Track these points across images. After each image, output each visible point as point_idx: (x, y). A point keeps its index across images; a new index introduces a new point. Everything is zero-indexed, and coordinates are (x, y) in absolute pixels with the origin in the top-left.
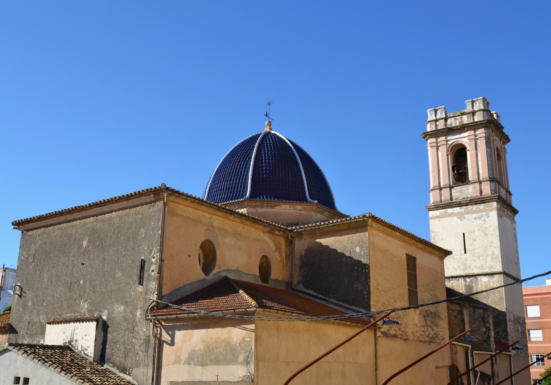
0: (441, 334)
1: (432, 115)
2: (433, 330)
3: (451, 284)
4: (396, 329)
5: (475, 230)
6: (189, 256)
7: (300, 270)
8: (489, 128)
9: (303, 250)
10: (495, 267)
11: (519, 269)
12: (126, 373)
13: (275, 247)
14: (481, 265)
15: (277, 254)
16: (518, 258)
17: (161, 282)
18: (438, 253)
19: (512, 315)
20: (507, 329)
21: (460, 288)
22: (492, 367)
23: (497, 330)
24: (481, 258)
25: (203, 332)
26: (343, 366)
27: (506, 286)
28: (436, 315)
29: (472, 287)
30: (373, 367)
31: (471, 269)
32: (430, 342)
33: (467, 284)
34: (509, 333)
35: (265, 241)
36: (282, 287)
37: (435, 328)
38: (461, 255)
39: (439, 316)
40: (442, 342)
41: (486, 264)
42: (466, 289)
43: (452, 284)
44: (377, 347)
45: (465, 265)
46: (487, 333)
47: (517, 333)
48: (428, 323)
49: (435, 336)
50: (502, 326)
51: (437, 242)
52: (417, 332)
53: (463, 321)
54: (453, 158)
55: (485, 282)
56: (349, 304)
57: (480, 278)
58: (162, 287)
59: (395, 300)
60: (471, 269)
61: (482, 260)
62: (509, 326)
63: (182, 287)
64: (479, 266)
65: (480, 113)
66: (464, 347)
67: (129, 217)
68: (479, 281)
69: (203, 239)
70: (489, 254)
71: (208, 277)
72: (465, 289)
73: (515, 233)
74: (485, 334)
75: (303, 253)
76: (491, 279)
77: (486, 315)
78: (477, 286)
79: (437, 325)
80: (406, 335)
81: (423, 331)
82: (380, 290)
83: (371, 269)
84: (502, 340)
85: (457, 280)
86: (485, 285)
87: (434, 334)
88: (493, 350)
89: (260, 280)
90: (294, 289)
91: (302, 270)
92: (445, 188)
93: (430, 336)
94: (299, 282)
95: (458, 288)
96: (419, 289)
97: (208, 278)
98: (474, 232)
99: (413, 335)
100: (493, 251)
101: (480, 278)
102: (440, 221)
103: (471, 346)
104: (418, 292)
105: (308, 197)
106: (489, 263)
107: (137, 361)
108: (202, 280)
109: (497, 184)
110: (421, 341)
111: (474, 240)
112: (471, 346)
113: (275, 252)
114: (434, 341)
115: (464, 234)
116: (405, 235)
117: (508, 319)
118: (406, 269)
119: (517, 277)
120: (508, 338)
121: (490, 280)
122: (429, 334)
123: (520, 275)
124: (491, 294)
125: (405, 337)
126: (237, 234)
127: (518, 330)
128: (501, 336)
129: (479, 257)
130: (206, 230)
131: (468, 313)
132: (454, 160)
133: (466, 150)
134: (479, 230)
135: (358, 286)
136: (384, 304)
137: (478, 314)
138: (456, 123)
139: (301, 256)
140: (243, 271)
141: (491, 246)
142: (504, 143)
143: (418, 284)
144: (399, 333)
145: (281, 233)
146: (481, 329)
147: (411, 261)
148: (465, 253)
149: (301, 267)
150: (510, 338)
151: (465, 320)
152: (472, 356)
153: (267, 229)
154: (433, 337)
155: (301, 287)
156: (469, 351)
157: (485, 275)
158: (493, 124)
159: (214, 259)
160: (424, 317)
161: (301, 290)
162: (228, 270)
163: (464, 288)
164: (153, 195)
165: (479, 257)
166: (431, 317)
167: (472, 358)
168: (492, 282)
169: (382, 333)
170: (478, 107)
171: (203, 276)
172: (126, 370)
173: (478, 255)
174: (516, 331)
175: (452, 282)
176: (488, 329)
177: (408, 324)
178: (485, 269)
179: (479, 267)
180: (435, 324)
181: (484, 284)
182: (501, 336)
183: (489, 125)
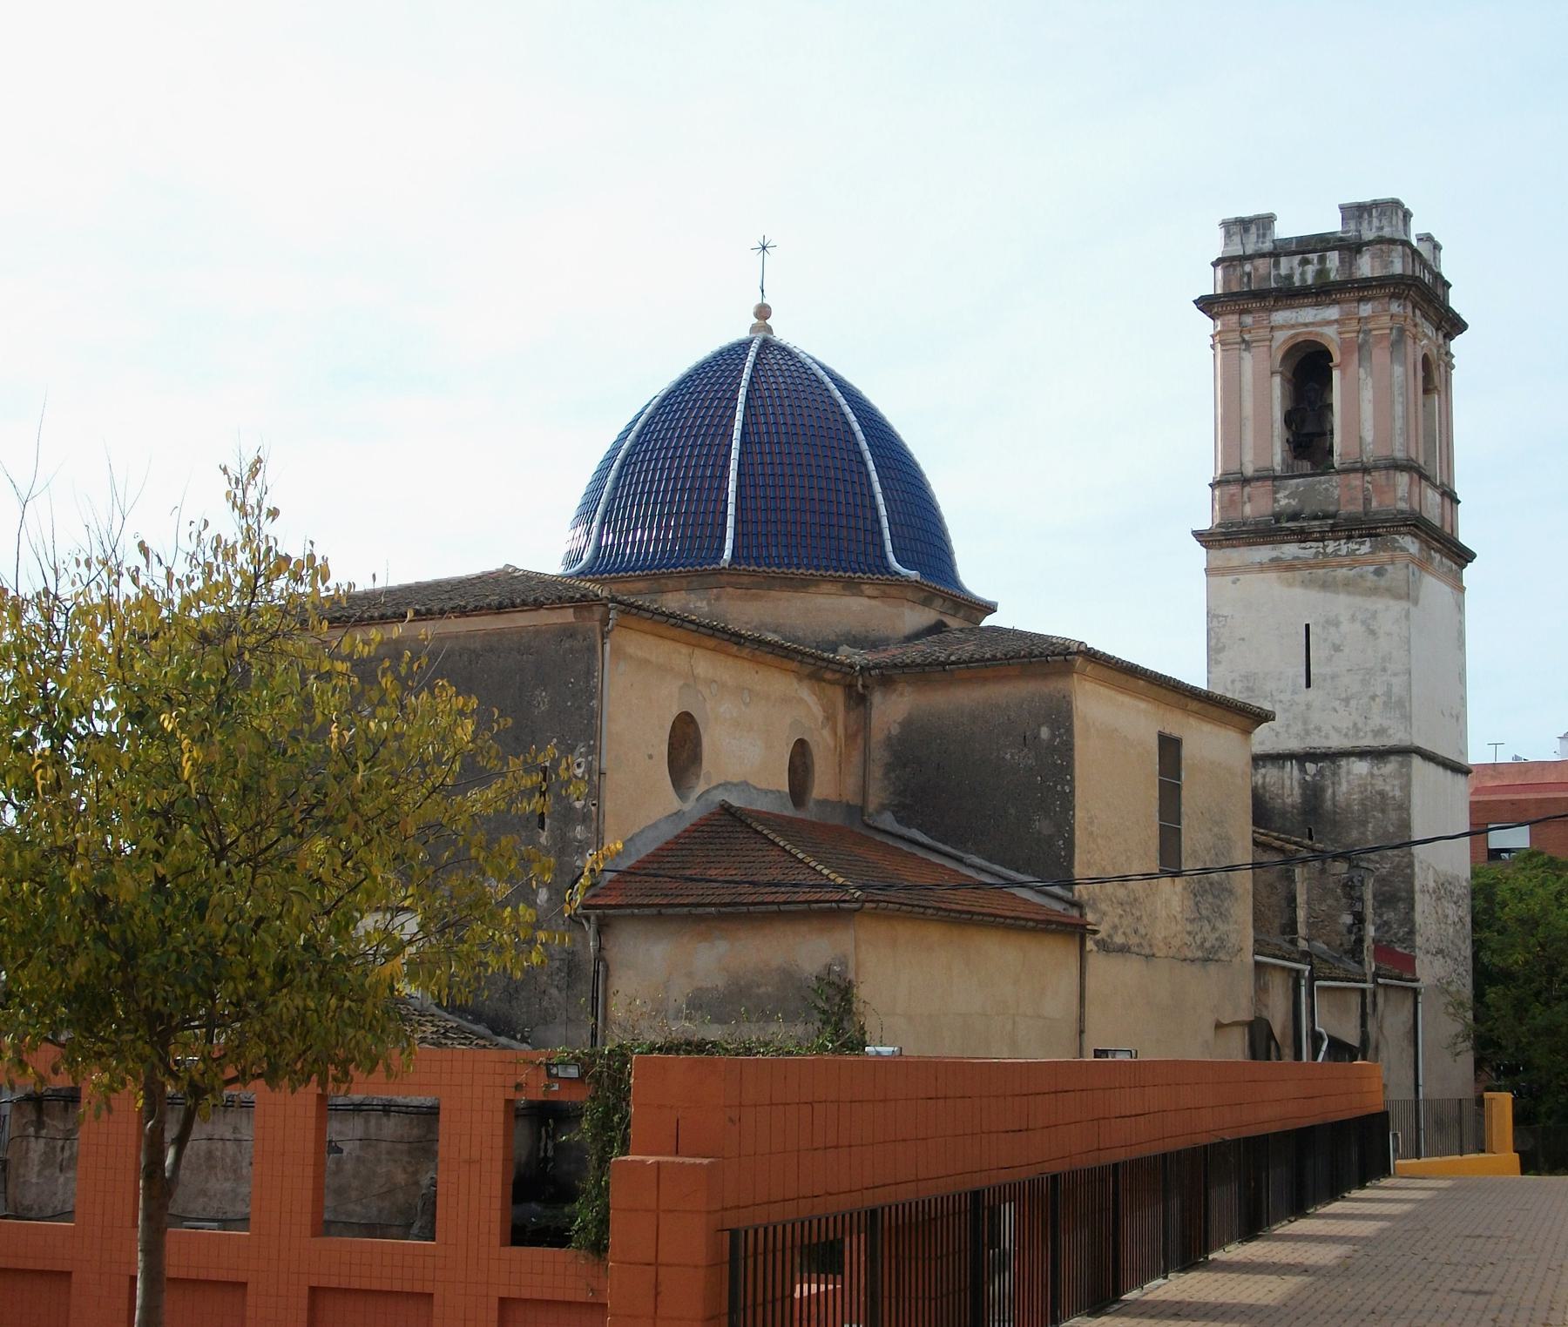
0: (1233, 938)
1: (1234, 237)
2: (1214, 929)
3: (1259, 776)
4: (1128, 931)
5: (1342, 619)
6: (651, 757)
7: (886, 775)
8: (1405, 299)
9: (895, 721)
10: (1391, 731)
11: (1462, 734)
12: (514, 1038)
13: (822, 713)
14: (1351, 725)
15: (826, 733)
16: (1463, 699)
17: (601, 827)
18: (1237, 719)
19: (1431, 871)
20: (1413, 916)
21: (1287, 791)
22: (1363, 1024)
23: (1385, 918)
24: (1353, 703)
25: (722, 946)
26: (1014, 1023)
27: (1407, 843)
28: (1226, 891)
29: (1323, 790)
30: (1075, 1027)
31: (1323, 734)
32: (1207, 960)
33: (1308, 778)
34: (1417, 926)
35: (801, 699)
36: (837, 820)
37: (1219, 924)
38: (1294, 692)
39: (1231, 892)
40: (1234, 960)
41: (1366, 724)
42: (1303, 795)
43: (1264, 777)
44: (1084, 979)
45: (1305, 723)
46: (1355, 930)
47: (1443, 926)
48: (1204, 912)
49: (1217, 944)
50: (1401, 906)
51: (1224, 647)
52: (1175, 936)
53: (1292, 900)
54: (1289, 381)
55: (1360, 776)
56: (1018, 870)
57: (1348, 764)
58: (603, 838)
59: (1128, 858)
60: (1323, 734)
61: (1357, 709)
62: (1418, 907)
63: (637, 835)
64: (1348, 728)
65: (1381, 250)
66: (1291, 969)
67: (499, 657)
68: (1343, 771)
69: (675, 712)
70: (1378, 693)
71: (686, 805)
72: (1301, 795)
73: (1461, 623)
74: (1350, 932)
75: (895, 730)
76: (1378, 769)
77: (1355, 880)
78: (1337, 786)
79: (1224, 916)
80: (1150, 946)
81: (1189, 933)
82: (1095, 834)
83: (1077, 783)
84: (1396, 945)
85: (1279, 768)
86: (1359, 785)
87: (1217, 939)
88: (1369, 978)
89: (790, 804)
90: (868, 826)
91: (892, 775)
92: (1258, 479)
93: (1207, 945)
94: (883, 808)
95: (1280, 792)
96: (1184, 822)
97: (687, 807)
98: (1337, 624)
99: (1165, 944)
100: (1390, 686)
101: (1348, 764)
102: (1238, 583)
103: (1309, 967)
104: (1183, 831)
105: (891, 558)
106: (1377, 721)
107: (546, 1009)
108: (675, 814)
109: (1416, 476)
110: (1185, 960)
111: (1337, 648)
112: (1309, 967)
113: (823, 726)
114: (1216, 958)
115: (1307, 626)
116: (1160, 686)
117: (1417, 887)
118: (1157, 773)
119: (1453, 756)
120: (1413, 941)
121: (1375, 771)
122: (1205, 940)
123: (1464, 752)
124: (1375, 813)
125: (1147, 951)
126: (743, 689)
127: (1446, 916)
128: (1396, 934)
129: (1347, 701)
130: (681, 688)
131: (1306, 875)
132: (1292, 389)
133: (1331, 364)
134: (1353, 618)
135: (1043, 826)
136: (1104, 869)
137: (1334, 875)
138: (1303, 274)
139: (889, 738)
140: (755, 784)
141: (1384, 670)
142: (1449, 336)
143: (1183, 809)
144: (1134, 940)
145: (838, 676)
146: (1339, 916)
147: (1170, 747)
148: (1308, 685)
149: (889, 768)
150: (1419, 940)
151: (1298, 896)
152: (1311, 995)
153: (808, 669)
154: (1213, 947)
155: (888, 821)
156: (1303, 982)
157: (1362, 754)
158: (1417, 286)
159: (696, 757)
160: (1195, 895)
161: (888, 828)
162: (725, 785)
163: (1297, 791)
164: (572, 610)
165: (1347, 701)
166: (1210, 896)
167: (1309, 1001)
168: (1381, 778)
169: (1097, 943)
170: (1374, 230)
171: (671, 802)
172: (514, 1030)
173: (1343, 696)
174: (1438, 919)
175: (1263, 771)
176: (1359, 919)
177: (1157, 918)
178: (1363, 738)
179: (1345, 731)
180: (1221, 914)
181: (1356, 782)
182: (1396, 934)
183: (1404, 291)
